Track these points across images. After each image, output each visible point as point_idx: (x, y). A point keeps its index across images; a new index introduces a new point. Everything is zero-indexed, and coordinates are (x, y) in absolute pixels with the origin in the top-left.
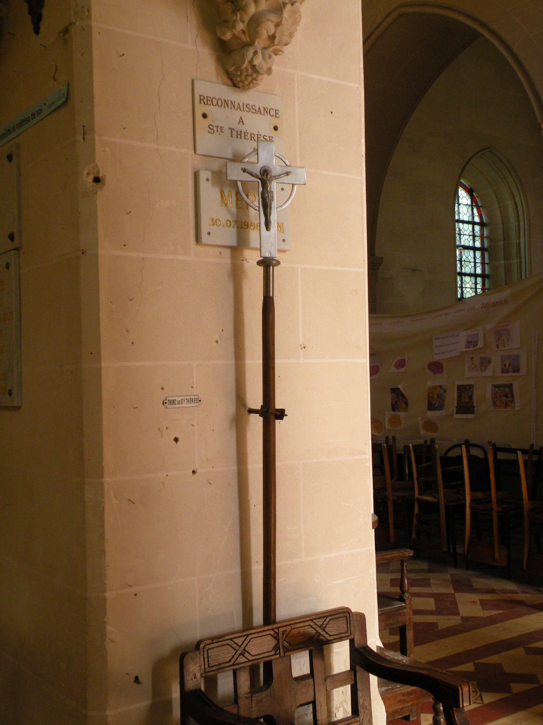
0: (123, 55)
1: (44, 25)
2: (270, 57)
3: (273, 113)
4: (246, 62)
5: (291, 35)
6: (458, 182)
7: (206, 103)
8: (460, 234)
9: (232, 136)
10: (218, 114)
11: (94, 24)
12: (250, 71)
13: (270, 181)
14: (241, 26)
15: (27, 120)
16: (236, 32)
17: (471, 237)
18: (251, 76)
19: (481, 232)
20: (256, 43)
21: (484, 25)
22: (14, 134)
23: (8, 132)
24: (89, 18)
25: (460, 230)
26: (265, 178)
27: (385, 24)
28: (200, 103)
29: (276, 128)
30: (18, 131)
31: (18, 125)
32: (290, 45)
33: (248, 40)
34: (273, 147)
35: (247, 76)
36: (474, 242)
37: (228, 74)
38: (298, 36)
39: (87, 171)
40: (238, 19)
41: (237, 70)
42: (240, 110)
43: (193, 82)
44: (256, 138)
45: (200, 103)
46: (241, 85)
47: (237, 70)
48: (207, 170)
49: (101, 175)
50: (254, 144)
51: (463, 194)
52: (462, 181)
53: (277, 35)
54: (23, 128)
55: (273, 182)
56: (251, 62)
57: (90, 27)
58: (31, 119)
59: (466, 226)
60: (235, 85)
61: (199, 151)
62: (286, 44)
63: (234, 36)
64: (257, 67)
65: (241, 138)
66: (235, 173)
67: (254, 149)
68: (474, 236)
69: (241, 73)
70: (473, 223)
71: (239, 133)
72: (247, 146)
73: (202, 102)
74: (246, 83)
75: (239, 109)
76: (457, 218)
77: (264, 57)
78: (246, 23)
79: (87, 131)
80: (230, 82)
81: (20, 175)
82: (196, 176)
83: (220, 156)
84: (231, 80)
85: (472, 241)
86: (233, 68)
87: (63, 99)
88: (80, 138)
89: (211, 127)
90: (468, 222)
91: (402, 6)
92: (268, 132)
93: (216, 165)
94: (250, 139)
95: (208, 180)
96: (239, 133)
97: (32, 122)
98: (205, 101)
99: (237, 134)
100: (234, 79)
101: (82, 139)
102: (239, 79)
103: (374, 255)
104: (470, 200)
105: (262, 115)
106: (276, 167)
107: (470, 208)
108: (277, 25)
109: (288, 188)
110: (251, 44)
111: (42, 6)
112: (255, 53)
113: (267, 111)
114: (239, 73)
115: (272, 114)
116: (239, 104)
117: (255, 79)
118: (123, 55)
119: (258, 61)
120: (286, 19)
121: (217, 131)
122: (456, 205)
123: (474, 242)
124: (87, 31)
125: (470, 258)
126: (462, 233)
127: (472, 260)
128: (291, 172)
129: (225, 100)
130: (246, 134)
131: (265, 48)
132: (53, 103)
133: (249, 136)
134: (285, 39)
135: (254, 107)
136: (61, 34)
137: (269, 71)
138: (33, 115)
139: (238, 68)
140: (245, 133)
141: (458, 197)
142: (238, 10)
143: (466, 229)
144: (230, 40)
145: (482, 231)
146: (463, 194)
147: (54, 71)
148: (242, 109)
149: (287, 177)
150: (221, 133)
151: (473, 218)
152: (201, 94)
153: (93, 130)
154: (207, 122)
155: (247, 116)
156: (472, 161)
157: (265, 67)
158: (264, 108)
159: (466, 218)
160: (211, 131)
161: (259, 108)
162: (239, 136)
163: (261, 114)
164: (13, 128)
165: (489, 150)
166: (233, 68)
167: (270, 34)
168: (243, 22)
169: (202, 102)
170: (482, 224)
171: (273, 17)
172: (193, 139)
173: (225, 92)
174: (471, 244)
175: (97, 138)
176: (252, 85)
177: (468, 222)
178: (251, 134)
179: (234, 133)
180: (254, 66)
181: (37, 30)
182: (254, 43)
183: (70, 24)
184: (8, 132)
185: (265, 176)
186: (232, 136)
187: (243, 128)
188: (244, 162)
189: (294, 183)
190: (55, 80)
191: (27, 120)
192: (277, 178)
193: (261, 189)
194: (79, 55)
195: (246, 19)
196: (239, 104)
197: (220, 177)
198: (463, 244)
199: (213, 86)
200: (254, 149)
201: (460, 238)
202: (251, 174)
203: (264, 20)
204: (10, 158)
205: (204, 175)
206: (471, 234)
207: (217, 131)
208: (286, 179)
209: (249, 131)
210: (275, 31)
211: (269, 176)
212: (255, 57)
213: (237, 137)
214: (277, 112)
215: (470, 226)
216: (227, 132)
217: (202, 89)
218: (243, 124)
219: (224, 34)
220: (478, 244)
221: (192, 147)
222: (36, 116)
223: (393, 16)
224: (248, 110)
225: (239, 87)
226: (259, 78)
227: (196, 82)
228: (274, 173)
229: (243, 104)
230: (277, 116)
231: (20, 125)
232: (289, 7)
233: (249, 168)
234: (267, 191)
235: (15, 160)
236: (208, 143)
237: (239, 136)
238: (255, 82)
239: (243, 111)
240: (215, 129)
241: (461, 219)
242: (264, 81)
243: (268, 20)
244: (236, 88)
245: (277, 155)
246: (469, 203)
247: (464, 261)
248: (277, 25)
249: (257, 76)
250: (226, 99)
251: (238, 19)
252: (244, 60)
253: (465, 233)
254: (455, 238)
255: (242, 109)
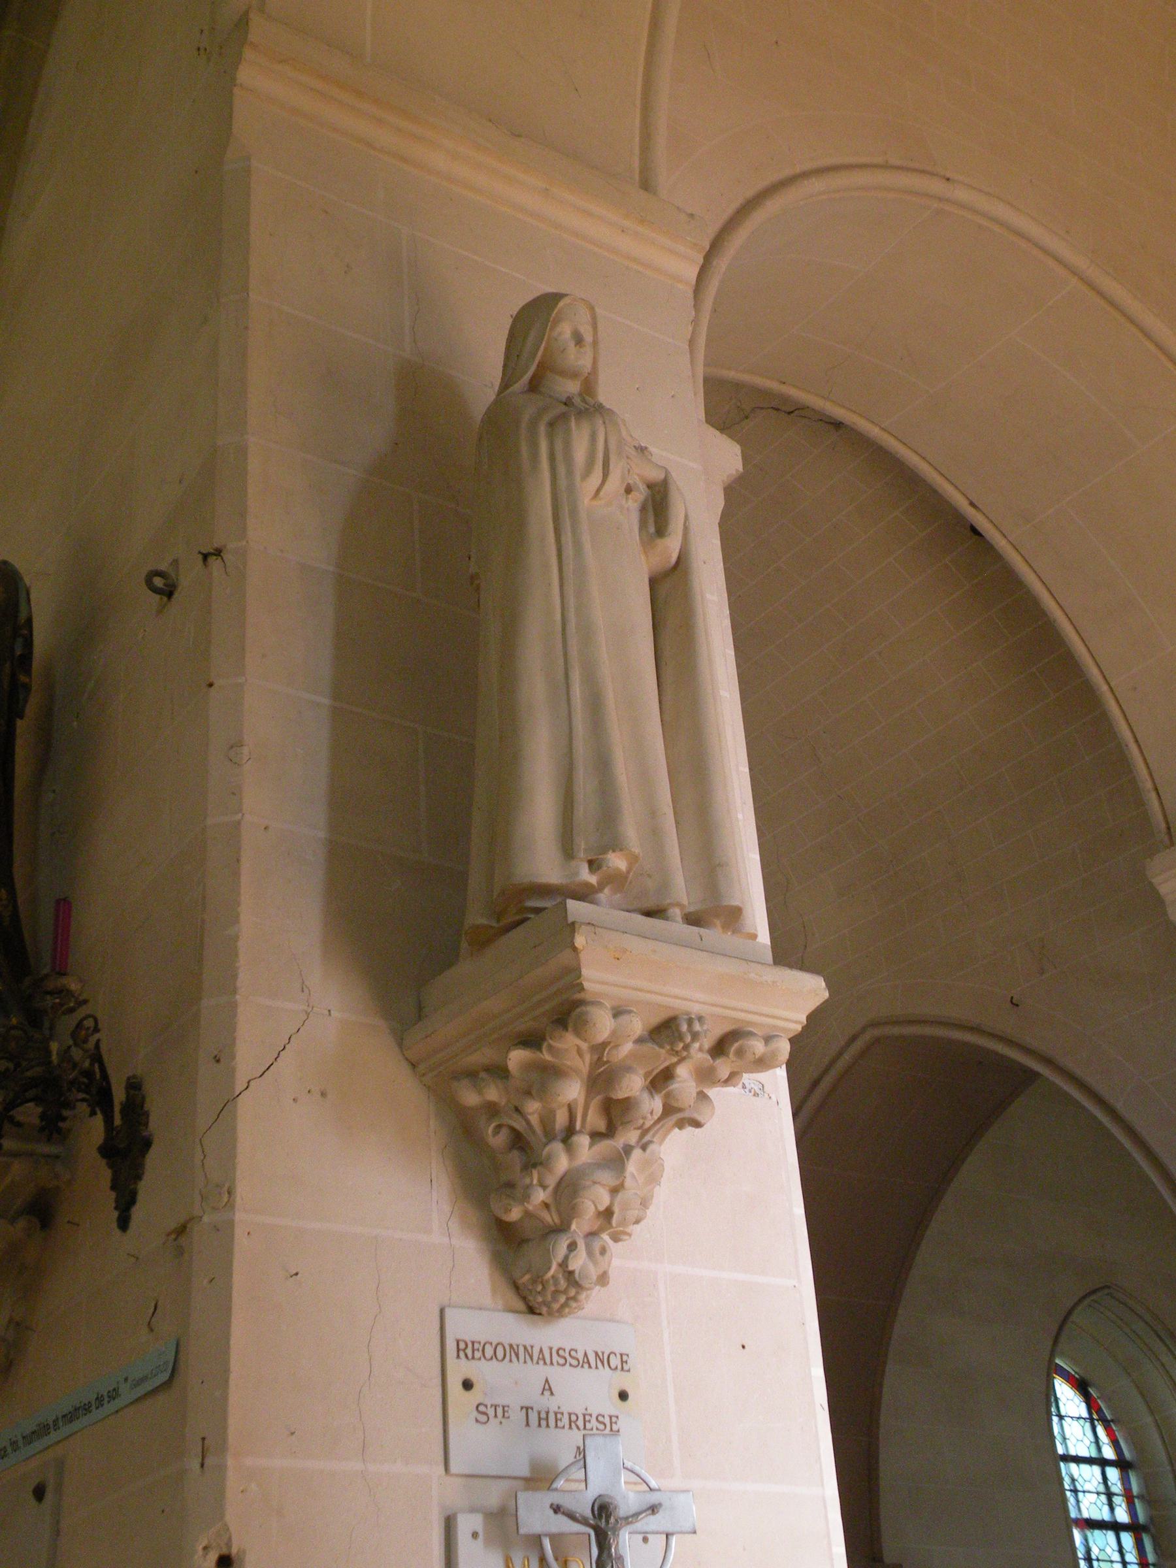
0: (297, 1274)
1: (138, 1213)
2: (603, 1251)
3: (615, 1361)
4: (554, 1267)
5: (645, 1203)
6: (1049, 1368)
7: (470, 1356)
8: (1075, 1491)
9: (528, 1424)
10: (498, 1380)
11: (239, 1216)
12: (563, 1284)
13: (615, 1530)
14: (540, 1195)
15: (86, 1408)
16: (531, 1208)
17: (1103, 1498)
18: (565, 1292)
19: (1123, 1484)
20: (573, 1227)
21: (1048, 1061)
22: (54, 1436)
23: (43, 1430)
24: (230, 1205)
25: (1073, 1480)
26: (603, 1524)
27: (847, 1057)
28: (458, 1356)
29: (623, 1396)
30: (65, 1430)
31: (64, 1416)
32: (642, 1223)
33: (557, 1220)
34: (621, 1448)
35: (556, 1292)
36: (1112, 1509)
37: (516, 1287)
38: (662, 1193)
39: (204, 1544)
40: (535, 1182)
41: (534, 1282)
42: (545, 1363)
43: (442, 1311)
44: (580, 1423)
45: (458, 1356)
46: (544, 1310)
47: (534, 1282)
48: (473, 1510)
49: (234, 1551)
50: (576, 1437)
51: (1064, 1391)
52: (1058, 1361)
53: (616, 1209)
54: (76, 1425)
55: (621, 1532)
56: (564, 1264)
57: (231, 1224)
58: (94, 1407)
59: (1085, 1468)
60: (532, 1311)
61: (454, 1469)
62: (637, 1222)
63: (527, 1214)
64: (577, 1275)
65: (548, 1426)
66: (535, 1515)
67: (578, 1448)
68: (1110, 1495)
69: (544, 1287)
70: (1103, 1463)
71: (543, 1415)
72: (560, 1446)
73: (462, 1354)
74: (556, 1306)
75: (541, 1362)
76: (1060, 1450)
77: (590, 1253)
78: (550, 1189)
79: (210, 1449)
80: (521, 1306)
81: (58, 1533)
82: (449, 1525)
83: (500, 1473)
84: (524, 1299)
85: (1106, 1508)
86: (527, 1277)
87: (165, 1377)
88: (195, 1464)
89: (482, 1408)
90: (1089, 1461)
91: (874, 1024)
92: (606, 1404)
93: (493, 1496)
94: (567, 1426)
95: (475, 1535)
96: (543, 1415)
97: (96, 1414)
98: (469, 1352)
99: (540, 1419)
100: (531, 1298)
101: (198, 1466)
102: (540, 1299)
103: (881, 1560)
104: (1083, 1405)
105: (593, 1370)
106: (628, 1498)
107: (1088, 1425)
108: (614, 1191)
109: (658, 1541)
110: (562, 1228)
111: (139, 1177)
112: (572, 1246)
113: (603, 1359)
114: (539, 1288)
115: (613, 1365)
116: (541, 1350)
117: (574, 1299)
118: (297, 1274)
119: (578, 1262)
120: (633, 1176)
121: (496, 1416)
122: (1055, 1419)
123: (1112, 1509)
124: (225, 1231)
125: (1109, 1550)
126: (1079, 1488)
127: (1116, 1557)
128: (660, 1505)
129: (511, 1346)
130: (559, 1416)
131: (592, 1235)
132: (144, 1379)
133: (566, 1420)
134: (633, 1214)
135: (573, 1353)
136: (173, 1236)
137: (603, 1279)
138: (100, 1400)
139: (538, 1279)
140: (556, 1414)
141: (1057, 1400)
142: (535, 1166)
143: (1087, 1476)
144: (521, 1220)
145: (1125, 1480)
146: (1064, 1391)
147: (152, 1310)
148: (548, 1361)
149: (652, 1517)
150: (503, 1421)
151: (1099, 1449)
152: (459, 1337)
153: (223, 1448)
154: (474, 1396)
155: (559, 1375)
156: (1074, 1317)
157: (593, 1272)
158: (597, 1354)
159: (1084, 1453)
160: (483, 1418)
161: (586, 1354)
162: (543, 1423)
163: (590, 1367)
164: (55, 1421)
165: (1106, 1291)
166: (527, 1277)
167: (602, 1208)
168: (544, 1187)
169: (462, 1354)
170: (1122, 1464)
171: (606, 1177)
172: (442, 1445)
173: (515, 1329)
174: (1105, 1515)
175: (230, 1462)
176: (567, 1310)
177: (1089, 1461)
178: (570, 1414)
179: (533, 1417)
180: (571, 1273)
181: (124, 1223)
182: (569, 1227)
183: (192, 1219)
184: (43, 1430)
185: (603, 1519)
186: (528, 1424)
187: (552, 1404)
188: (556, 1490)
189: (670, 1530)
190: (152, 1330)
191: (86, 1408)
192: (631, 1523)
193: (595, 1551)
194: (205, 1282)
195: (552, 1181)
196: (541, 1350)
197: (501, 1524)
198: (1086, 1515)
199: (486, 1318)
200: (578, 1448)
201: (1078, 1501)
202: (572, 1516)
203: (588, 1183)
204: (39, 1493)
205: (467, 1524)
206: (1102, 1488)
207: (496, 1416)
208: (650, 1523)
209: (565, 1409)
210: (612, 1204)
211: (612, 1520)
212: (572, 1255)
213: (540, 1425)
214: (625, 1358)
215: (1096, 1470)
216: (517, 1416)
217: (462, 1325)
218: (552, 1394)
219: (508, 1210)
220: (1122, 1516)
221: (441, 1458)
222: (105, 1402)
223: (859, 1044)
224: (562, 1361)
225: (540, 1314)
226: (583, 1296)
227: (449, 1313)
228: (622, 1511)
229: (551, 1349)
230: (626, 1367)
231: (70, 1417)
232: (637, 1153)
233: (567, 1503)
234: (610, 1555)
235: (49, 1496)
236: (477, 1445)
237: (543, 1423)
238: (574, 1304)
239: (552, 1363)
240: (491, 1412)
241: (1073, 1452)
242: (594, 1300)
243: (595, 1183)
244: (536, 1317)
245: (629, 1464)
246: (1085, 1414)
247: (1098, 1560)
248: (614, 1191)
249: (577, 1293)
250: (514, 1342)
251: (535, 1182)
252: (550, 1262)
253: (1087, 1487)
254: (1065, 1500)
255: (548, 1361)
